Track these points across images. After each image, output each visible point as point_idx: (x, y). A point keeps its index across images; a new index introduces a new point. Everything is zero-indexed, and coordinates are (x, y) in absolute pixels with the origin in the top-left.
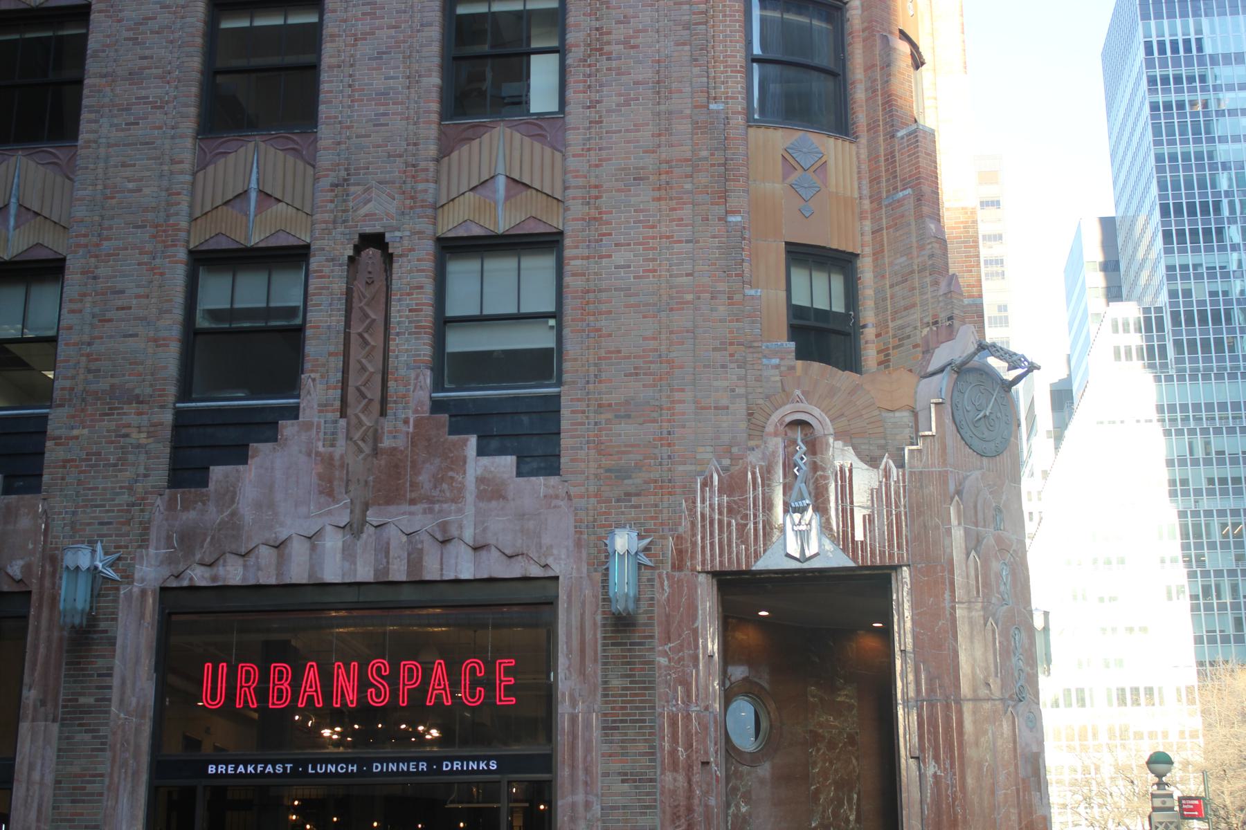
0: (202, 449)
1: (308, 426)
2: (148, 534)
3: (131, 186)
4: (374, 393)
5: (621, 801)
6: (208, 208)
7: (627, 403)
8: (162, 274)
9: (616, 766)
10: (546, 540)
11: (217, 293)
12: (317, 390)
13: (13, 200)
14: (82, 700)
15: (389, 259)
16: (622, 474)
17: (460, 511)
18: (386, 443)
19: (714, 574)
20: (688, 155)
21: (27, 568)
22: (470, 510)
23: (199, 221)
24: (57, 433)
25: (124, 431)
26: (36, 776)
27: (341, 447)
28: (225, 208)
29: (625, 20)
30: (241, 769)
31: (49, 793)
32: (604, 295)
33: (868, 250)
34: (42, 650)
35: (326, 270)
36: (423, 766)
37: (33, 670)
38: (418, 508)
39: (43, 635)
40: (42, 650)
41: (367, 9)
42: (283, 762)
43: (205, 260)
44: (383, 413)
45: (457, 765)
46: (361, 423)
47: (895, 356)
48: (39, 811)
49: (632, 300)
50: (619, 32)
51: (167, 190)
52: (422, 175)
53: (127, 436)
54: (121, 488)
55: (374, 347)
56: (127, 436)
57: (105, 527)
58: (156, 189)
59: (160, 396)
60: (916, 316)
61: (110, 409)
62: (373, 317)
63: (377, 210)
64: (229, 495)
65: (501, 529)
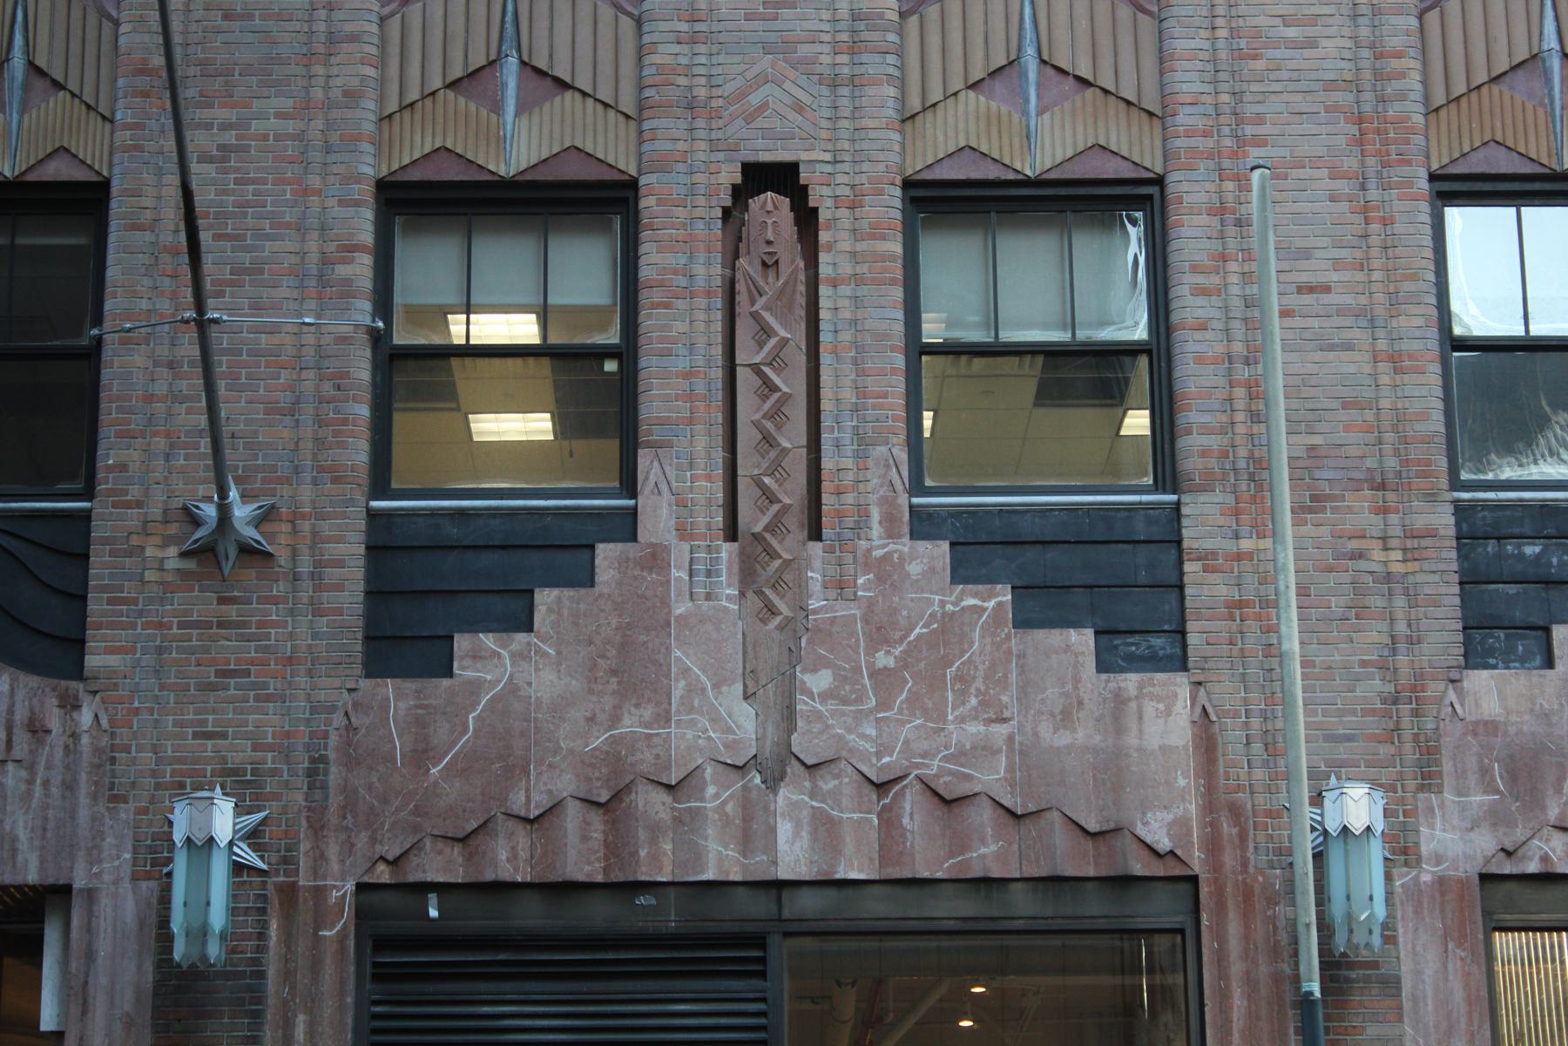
2: (1438, 763)
3: (1292, 32)
4: (793, 492)
8: (1386, 222)
13: (1030, 51)
15: (807, 219)
23: (1443, 112)
24: (1208, 544)
25: (1353, 545)
28: (1495, 88)
34: (1238, 1001)
39: (1236, 969)
40: (1238, 1001)
51: (1372, 46)
53: (1359, 555)
54: (1364, 664)
55: (788, 396)
56: (1359, 555)
57: (1341, 747)
58: (1348, 43)
59: (1420, 475)
61: (1314, 498)
62: (783, 333)
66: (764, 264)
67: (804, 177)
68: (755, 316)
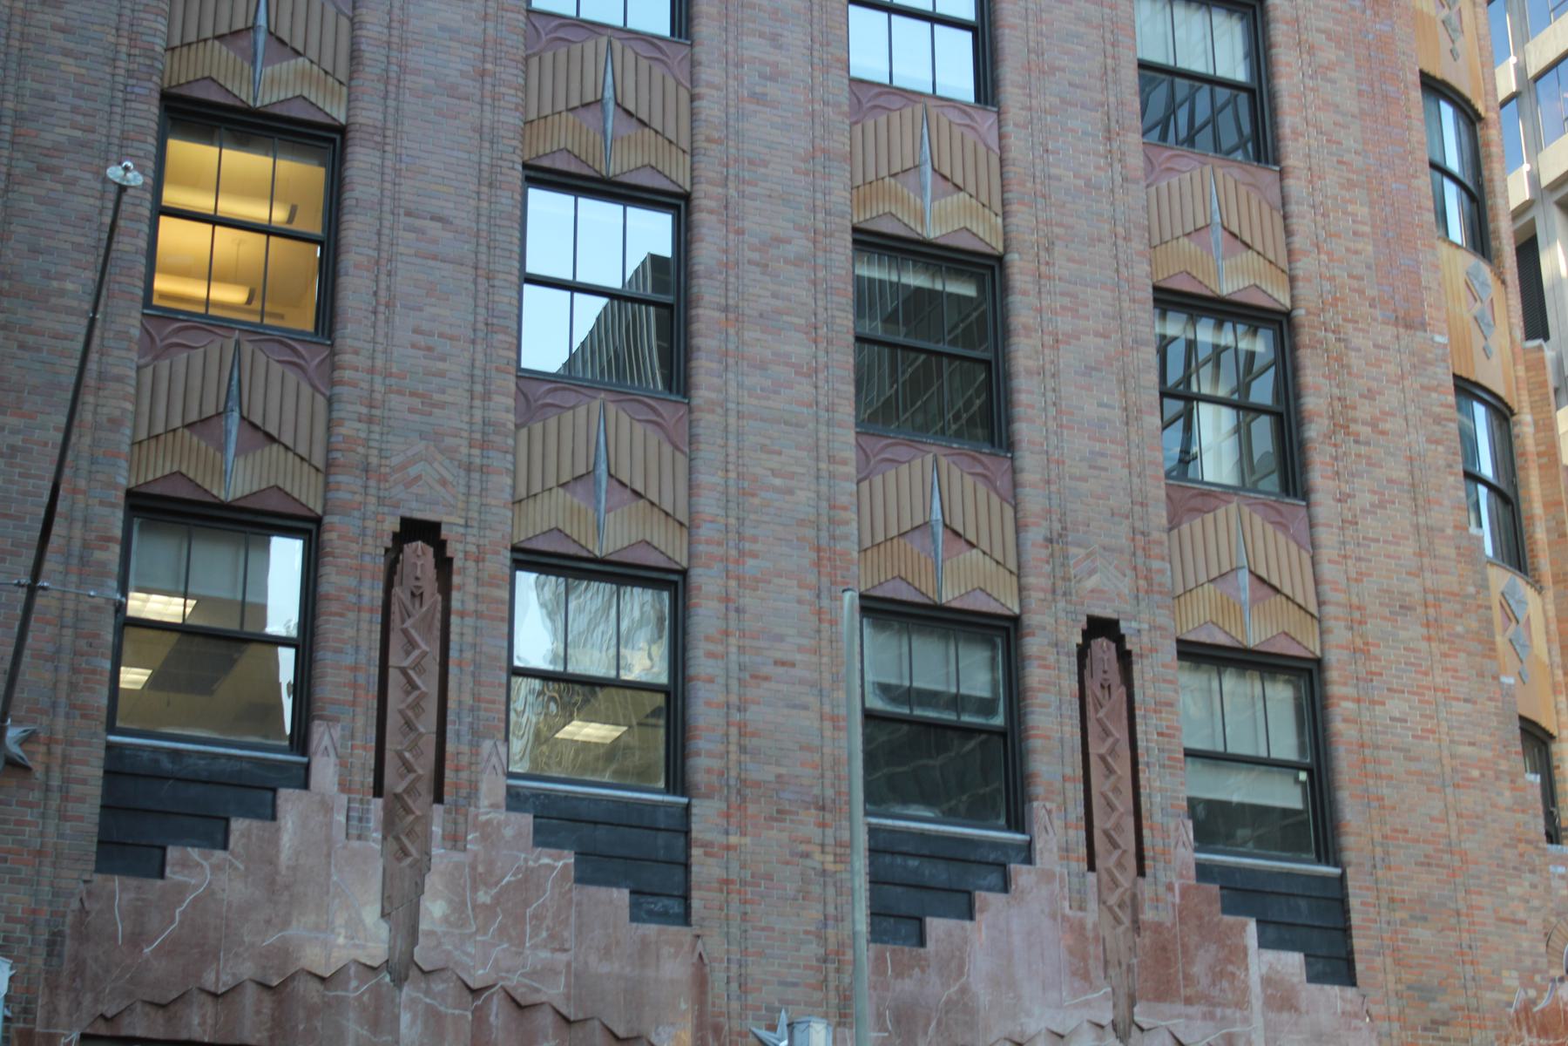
1: (1048, 876)
16: (1424, 994)
17: (1246, 1021)
18: (1148, 915)
20: (1456, 588)
22: (1258, 1020)
24: (708, 837)
27: (1092, 915)
29: (1370, 395)
32: (1382, 754)
35: (1052, 658)
44: (1141, 872)
46: (1116, 884)
49: (1413, 766)
50: (1365, 410)
52: (1156, 550)
63: (1105, 589)
64: (955, 964)
66: (413, 594)
67: (444, 533)
68: (405, 632)
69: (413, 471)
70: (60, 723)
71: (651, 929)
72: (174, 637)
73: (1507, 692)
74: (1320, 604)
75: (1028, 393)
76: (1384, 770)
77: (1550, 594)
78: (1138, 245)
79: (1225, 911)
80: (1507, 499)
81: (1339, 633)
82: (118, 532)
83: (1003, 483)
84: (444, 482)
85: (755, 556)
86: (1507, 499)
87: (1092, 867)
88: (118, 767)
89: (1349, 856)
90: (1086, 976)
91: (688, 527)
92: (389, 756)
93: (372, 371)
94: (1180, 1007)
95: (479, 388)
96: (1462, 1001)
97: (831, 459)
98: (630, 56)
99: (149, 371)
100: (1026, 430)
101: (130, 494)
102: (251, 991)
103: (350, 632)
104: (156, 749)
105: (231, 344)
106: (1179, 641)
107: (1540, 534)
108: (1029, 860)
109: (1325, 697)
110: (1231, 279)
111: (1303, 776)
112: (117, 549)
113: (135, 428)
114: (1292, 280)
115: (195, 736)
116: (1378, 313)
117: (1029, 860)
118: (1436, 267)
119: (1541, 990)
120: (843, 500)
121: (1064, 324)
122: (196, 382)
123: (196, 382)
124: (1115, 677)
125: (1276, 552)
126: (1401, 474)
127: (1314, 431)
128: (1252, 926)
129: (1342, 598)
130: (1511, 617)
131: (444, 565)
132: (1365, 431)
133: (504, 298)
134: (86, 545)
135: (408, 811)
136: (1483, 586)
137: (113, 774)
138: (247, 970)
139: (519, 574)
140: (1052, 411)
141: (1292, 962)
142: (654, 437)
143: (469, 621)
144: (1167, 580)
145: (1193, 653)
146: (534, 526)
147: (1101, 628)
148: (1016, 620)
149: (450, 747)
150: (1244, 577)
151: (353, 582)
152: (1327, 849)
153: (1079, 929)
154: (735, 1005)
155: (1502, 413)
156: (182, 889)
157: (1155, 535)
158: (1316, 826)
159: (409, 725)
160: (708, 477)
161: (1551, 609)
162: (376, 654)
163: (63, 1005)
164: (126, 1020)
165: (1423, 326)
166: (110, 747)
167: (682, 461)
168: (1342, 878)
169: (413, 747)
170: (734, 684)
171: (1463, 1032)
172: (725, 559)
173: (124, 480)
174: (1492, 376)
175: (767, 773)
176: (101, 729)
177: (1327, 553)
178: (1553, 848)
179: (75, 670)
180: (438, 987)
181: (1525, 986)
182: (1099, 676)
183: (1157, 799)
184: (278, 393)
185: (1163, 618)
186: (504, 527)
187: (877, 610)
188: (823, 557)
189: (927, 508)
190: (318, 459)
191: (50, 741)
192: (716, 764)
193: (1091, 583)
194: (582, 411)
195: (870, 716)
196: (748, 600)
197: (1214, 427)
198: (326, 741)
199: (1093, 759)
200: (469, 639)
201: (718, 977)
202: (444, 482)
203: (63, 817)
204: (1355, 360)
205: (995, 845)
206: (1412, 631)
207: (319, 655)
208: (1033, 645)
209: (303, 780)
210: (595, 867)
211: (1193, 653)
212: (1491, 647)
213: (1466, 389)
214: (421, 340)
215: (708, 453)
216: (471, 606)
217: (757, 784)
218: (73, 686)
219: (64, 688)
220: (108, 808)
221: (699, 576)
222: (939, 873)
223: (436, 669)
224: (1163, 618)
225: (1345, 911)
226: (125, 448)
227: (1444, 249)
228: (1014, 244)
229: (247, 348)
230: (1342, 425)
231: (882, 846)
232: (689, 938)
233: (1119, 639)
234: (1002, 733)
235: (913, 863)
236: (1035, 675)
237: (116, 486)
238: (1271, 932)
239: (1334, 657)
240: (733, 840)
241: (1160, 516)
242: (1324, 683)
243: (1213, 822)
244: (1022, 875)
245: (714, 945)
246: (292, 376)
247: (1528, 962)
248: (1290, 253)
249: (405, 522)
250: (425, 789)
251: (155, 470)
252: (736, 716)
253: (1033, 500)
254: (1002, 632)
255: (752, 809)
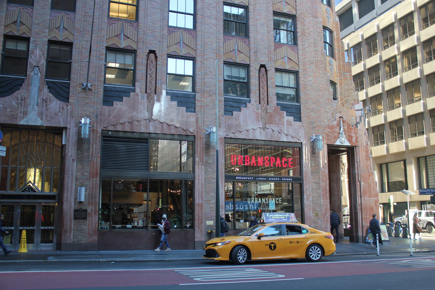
0: (231, 107)
1: (253, 105)
5: (315, 187)
6: (8, 24)
7: (312, 109)
9: (313, 181)
10: (300, 135)
11: (11, 45)
12: (254, 97)
14: (209, 161)
16: (312, 123)
17: (284, 127)
18: (269, 111)
19: (328, 145)
20: (321, 60)
21: (194, 130)
22: (285, 127)
24: (198, 99)
26: (200, 178)
27: (260, 111)
29: (308, 29)
30: (243, 178)
31: (203, 182)
32: (307, 86)
33: (338, 83)
35: (254, 71)
36: (278, 179)
37: (197, 154)
38: (276, 125)
39: (199, 146)
41: (258, 13)
42: (251, 177)
43: (7, 37)
44: (268, 104)
45: (285, 179)
46: (264, 106)
47: (345, 105)
48: (202, 185)
49: (312, 88)
50: (307, 31)
52: (272, 54)
60: (350, 98)
63: (264, 60)
64: (237, 118)
65: (291, 132)
69: (151, 42)
70: (96, 83)
71: (189, 113)
72: (173, 76)
73: (328, 76)
74: (298, 62)
75: (252, 28)
76: (307, 88)
77: (337, 61)
78: (270, 4)
79: (281, 110)
80: (331, 46)
81: (301, 67)
82: (105, 53)
83: (247, 43)
84: (156, 44)
85: (206, 55)
86: (331, 46)
87: (260, 104)
88: (106, 90)
89: (301, 102)
90: (258, 120)
91: (195, 50)
92: (148, 87)
93: (144, 26)
94: (273, 125)
95: (161, 29)
96: (318, 124)
97: (219, 39)
98: (66, 17)
99: (109, 28)
100: (251, 35)
101: (106, 47)
102: (127, 123)
103: (141, 68)
104: (111, 87)
105: (122, 23)
106: (275, 68)
107: (336, 51)
108: (250, 103)
109: (299, 77)
110: (286, 10)
111: (295, 89)
112: (104, 56)
113: (107, 37)
114: (296, 10)
115: (121, 85)
116: (310, 15)
117: (250, 103)
118: (320, 8)
119: (331, 122)
120: (221, 46)
121: (258, 17)
122: (116, 29)
123: (116, 29)
124: (265, 74)
125: (292, 54)
126: (313, 41)
127: (299, 35)
128: (285, 112)
129: (302, 61)
130: (330, 64)
131: (156, 57)
132: (307, 35)
133: (166, 14)
134: (99, 55)
135: (151, 96)
136: (325, 59)
137: (105, 91)
138: (126, 120)
139: (169, 59)
140: (256, 31)
141: (291, 118)
142: (190, 36)
143: (160, 66)
144: (274, 58)
145: (277, 70)
146: (171, 51)
147: (262, 66)
148: (249, 65)
149: (157, 86)
150: (286, 58)
151: (141, 60)
152: (298, 100)
153: (257, 113)
154: (202, 125)
155: (331, 32)
156: (116, 108)
157: (272, 51)
158: (297, 98)
159: (151, 82)
160: (199, 43)
161: (337, 64)
162: (145, 71)
163: (99, 125)
164: (108, 128)
165: (317, 18)
166: (104, 86)
167: (195, 40)
168: (300, 105)
169: (151, 86)
170: (203, 75)
171: (318, 129)
172: (201, 56)
173: (105, 45)
174: (329, 26)
175: (208, 89)
176: (103, 84)
177: (300, 54)
178: (334, 101)
179: (98, 75)
180: (156, 122)
181: (328, 122)
182: (262, 74)
183: (271, 93)
184: (129, 30)
185: (273, 65)
186: (166, 51)
187: (226, 63)
188: (218, 55)
189: (235, 47)
190: (136, 41)
191: (95, 86)
192: (200, 88)
193: (261, 59)
194: (178, 32)
195: (225, 80)
196: (205, 62)
197: (283, 34)
198: (138, 85)
199: (261, 87)
200: (160, 69)
201: (200, 121)
202: (156, 44)
203: (97, 97)
204: (306, 23)
205: (244, 100)
206: (313, 67)
207: (137, 72)
208: (251, 69)
209: (134, 91)
210: (180, 104)
211: (277, 70)
212: (326, 69)
213: (325, 28)
214: (152, 21)
215: (199, 38)
216: (160, 63)
217: (206, 91)
218: (98, 77)
219: (97, 77)
220: (104, 96)
221: (197, 58)
222: (235, 104)
223: (155, 73)
224: (273, 65)
225: (300, 110)
226: (105, 40)
227: (322, 5)
228: (250, 4)
229: (124, 23)
230: (303, 34)
231: (226, 100)
232: (195, 115)
233: (265, 68)
234: (246, 83)
235: (231, 103)
236: (252, 74)
237: (104, 46)
238: (288, 114)
239: (300, 71)
240: (202, 99)
241: (273, 48)
242: (299, 75)
243: (279, 97)
244: (248, 105)
245: (199, 116)
246: (131, 27)
247: (329, 118)
248: (296, 5)
249: (150, 50)
250: (153, 92)
251: (110, 43)
252: (203, 80)
253: (252, 46)
254: (247, 67)
255: (205, 95)
